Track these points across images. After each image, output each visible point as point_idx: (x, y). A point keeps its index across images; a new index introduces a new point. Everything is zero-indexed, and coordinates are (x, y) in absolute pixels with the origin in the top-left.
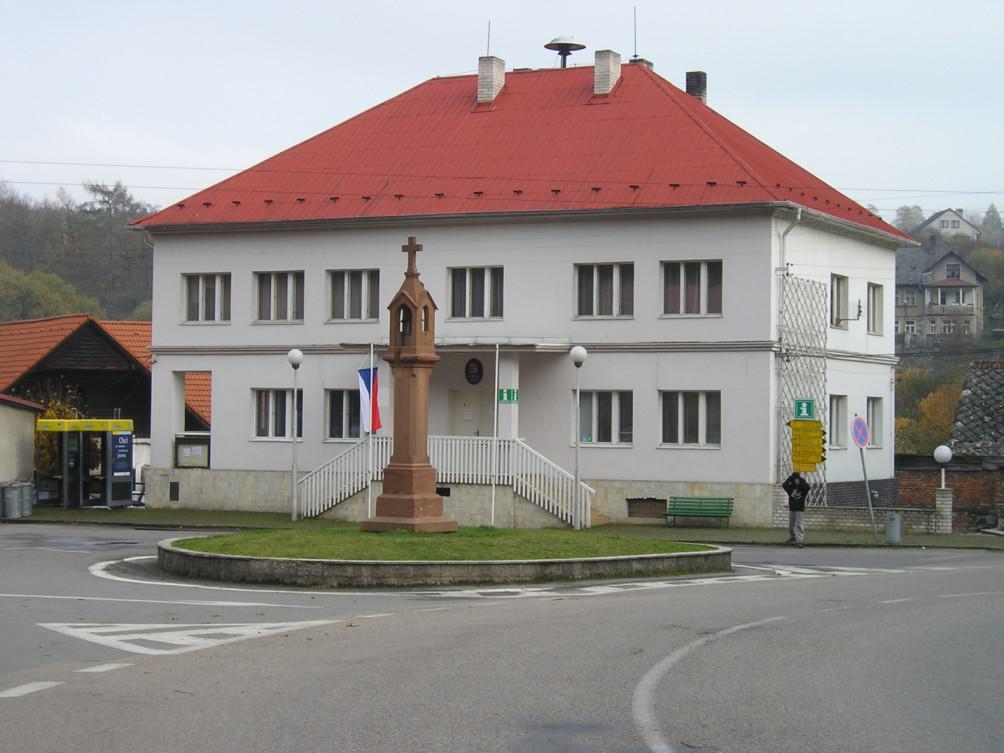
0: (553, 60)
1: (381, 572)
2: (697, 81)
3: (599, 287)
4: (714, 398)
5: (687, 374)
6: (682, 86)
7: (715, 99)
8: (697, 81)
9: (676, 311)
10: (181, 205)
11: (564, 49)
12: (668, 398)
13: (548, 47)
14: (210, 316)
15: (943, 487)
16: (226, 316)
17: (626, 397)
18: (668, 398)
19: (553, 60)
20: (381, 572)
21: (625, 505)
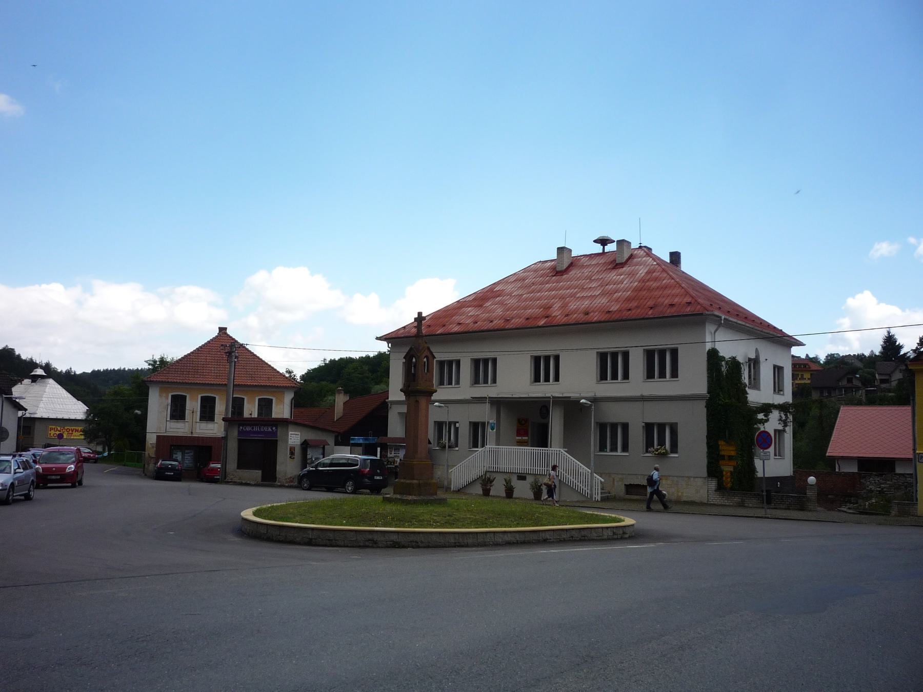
0: (598, 249)
1: (583, 533)
2: (675, 257)
3: (610, 366)
4: (674, 428)
5: (657, 414)
6: (667, 259)
7: (686, 266)
8: (675, 257)
9: (479, 383)
10: (404, 327)
11: (604, 242)
12: (649, 427)
13: (595, 241)
14: (615, 377)
15: (219, 466)
16: (458, 382)
17: (625, 426)
18: (649, 427)
19: (598, 249)
20: (583, 533)
21: (623, 487)
